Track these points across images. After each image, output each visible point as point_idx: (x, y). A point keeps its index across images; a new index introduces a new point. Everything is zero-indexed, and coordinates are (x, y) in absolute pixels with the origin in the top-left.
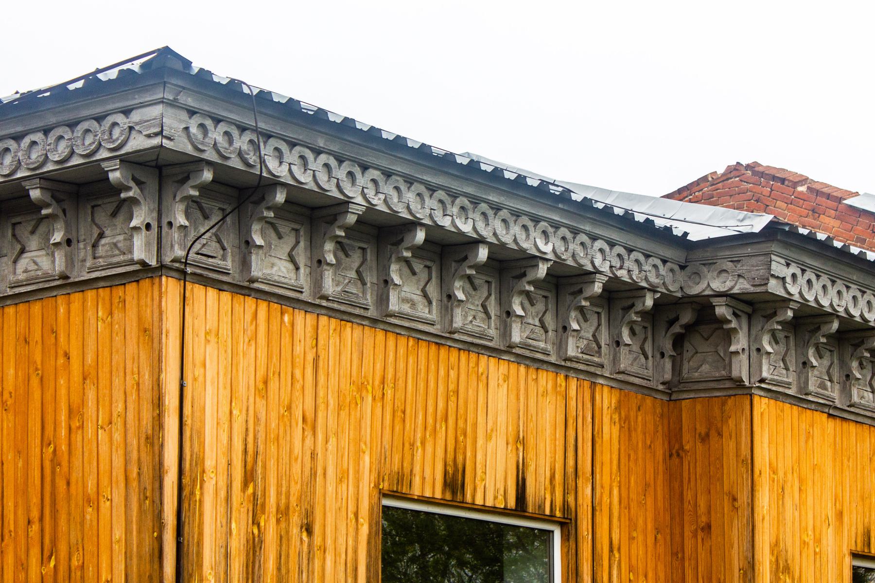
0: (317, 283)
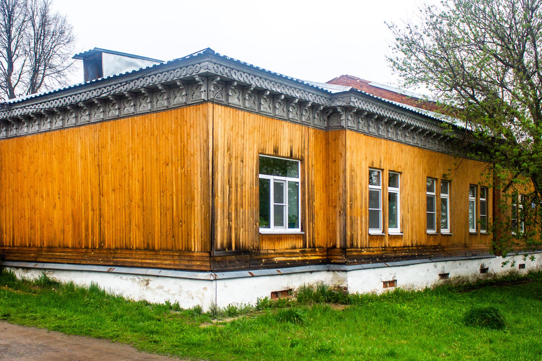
0: (244, 104)
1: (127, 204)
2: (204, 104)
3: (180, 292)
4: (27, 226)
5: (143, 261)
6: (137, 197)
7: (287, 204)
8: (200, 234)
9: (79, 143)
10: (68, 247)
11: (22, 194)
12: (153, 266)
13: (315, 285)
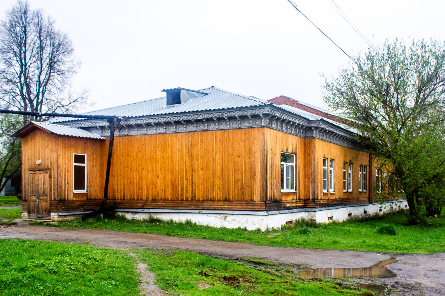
0: (277, 127)
1: (211, 176)
2: (263, 128)
3: (247, 221)
4: (136, 188)
5: (222, 207)
6: (218, 173)
7: (290, 177)
8: (259, 192)
9: (177, 142)
10: (168, 200)
11: (131, 169)
12: (229, 209)
13: (300, 219)
